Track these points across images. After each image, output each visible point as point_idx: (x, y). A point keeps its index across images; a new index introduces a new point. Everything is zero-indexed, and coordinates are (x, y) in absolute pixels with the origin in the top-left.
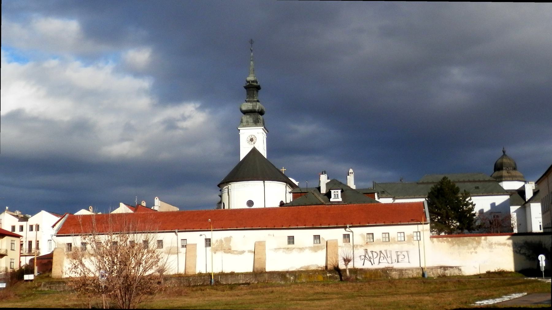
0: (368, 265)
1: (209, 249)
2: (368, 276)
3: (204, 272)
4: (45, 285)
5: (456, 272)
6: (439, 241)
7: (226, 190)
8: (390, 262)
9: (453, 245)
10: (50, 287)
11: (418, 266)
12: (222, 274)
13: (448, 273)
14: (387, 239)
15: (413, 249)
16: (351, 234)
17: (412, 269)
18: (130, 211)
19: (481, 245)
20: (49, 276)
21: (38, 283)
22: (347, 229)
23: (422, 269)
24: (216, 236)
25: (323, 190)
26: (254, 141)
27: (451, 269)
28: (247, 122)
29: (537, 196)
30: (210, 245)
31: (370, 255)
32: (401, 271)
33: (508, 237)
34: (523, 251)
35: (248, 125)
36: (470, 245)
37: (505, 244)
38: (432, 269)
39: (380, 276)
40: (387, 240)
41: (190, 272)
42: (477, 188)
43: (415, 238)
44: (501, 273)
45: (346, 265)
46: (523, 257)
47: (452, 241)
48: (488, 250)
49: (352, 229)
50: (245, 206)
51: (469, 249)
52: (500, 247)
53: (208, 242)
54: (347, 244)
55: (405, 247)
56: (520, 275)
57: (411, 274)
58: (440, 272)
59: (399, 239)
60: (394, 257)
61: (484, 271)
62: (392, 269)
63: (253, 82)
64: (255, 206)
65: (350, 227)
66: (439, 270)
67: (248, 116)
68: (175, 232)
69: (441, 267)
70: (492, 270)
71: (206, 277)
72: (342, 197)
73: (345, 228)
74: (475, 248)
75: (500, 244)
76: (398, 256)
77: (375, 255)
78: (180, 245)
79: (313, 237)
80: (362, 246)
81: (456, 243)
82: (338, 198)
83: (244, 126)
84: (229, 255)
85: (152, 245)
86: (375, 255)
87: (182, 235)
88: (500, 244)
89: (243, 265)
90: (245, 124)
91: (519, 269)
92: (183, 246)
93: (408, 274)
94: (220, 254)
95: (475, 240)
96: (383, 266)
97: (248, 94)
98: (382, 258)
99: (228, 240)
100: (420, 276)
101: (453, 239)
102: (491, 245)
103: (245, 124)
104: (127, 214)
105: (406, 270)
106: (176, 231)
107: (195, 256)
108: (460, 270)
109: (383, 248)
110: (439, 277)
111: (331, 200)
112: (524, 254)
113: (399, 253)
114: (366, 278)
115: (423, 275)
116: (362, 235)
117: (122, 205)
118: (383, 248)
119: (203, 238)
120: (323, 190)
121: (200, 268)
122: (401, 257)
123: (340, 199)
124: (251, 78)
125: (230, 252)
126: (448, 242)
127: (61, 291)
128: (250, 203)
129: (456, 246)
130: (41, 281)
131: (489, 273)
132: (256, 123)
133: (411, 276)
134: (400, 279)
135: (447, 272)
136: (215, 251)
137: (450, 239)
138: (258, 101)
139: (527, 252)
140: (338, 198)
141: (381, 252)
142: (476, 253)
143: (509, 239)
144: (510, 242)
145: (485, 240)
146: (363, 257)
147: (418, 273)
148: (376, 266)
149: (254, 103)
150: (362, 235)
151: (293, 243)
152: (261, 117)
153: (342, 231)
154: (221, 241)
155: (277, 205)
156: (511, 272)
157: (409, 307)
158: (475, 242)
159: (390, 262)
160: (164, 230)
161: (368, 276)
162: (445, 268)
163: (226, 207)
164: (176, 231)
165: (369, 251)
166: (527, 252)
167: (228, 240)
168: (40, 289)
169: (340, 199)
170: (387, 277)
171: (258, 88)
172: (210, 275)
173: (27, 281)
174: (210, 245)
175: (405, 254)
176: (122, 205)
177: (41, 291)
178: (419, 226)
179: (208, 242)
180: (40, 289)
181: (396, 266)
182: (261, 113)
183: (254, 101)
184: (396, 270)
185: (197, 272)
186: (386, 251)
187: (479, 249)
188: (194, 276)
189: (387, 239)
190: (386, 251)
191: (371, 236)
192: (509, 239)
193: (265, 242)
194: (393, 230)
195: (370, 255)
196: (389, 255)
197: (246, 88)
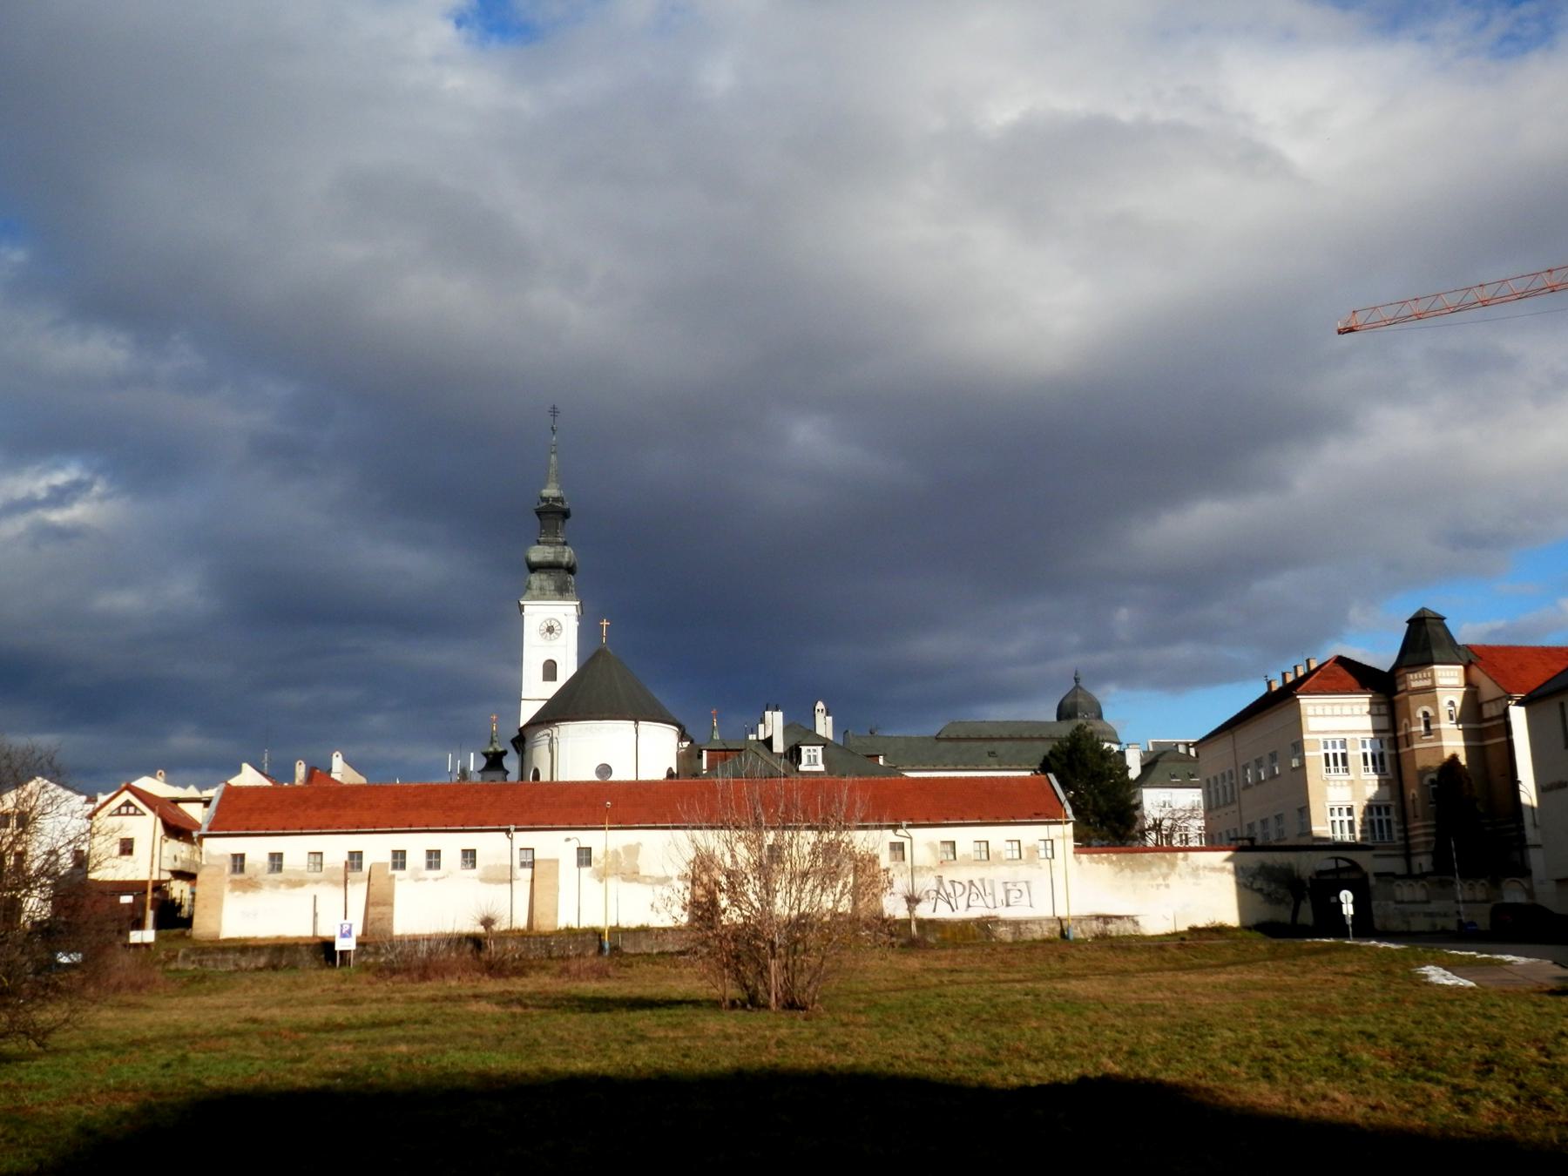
0: (943, 913)
1: (585, 870)
2: (948, 935)
3: (575, 926)
4: (186, 957)
5: (1128, 928)
6: (1093, 861)
7: (546, 740)
8: (991, 904)
9: (1122, 870)
10: (200, 962)
11: (1050, 914)
12: (616, 931)
13: (1113, 929)
14: (986, 854)
15: (1037, 876)
16: (907, 843)
17: (1038, 922)
18: (266, 783)
19: (1177, 870)
20: (183, 934)
21: (168, 951)
22: (900, 832)
23: (1060, 920)
24: (600, 841)
25: (779, 746)
26: (556, 628)
27: (1119, 922)
28: (541, 589)
29: (1154, 775)
30: (589, 863)
31: (950, 889)
32: (1016, 924)
33: (1228, 854)
34: (1257, 885)
35: (542, 595)
36: (1155, 870)
37: (1222, 869)
38: (1079, 920)
39: (974, 937)
40: (984, 856)
41: (544, 924)
42: (992, 754)
43: (1042, 854)
44: (1219, 931)
45: (911, 910)
46: (1259, 897)
47: (1119, 860)
48: (1190, 880)
49: (912, 831)
50: (593, 777)
51: (1153, 878)
52: (1213, 874)
53: (469, 856)
54: (472, 872)
55: (1023, 872)
56: (1259, 934)
57: (1039, 933)
58: (1096, 926)
59: (1009, 856)
60: (1000, 895)
61: (1183, 927)
62: (996, 921)
63: (556, 499)
64: (614, 778)
65: (909, 826)
66: (1094, 923)
67: (544, 576)
68: (508, 831)
69: (1098, 917)
70: (1201, 924)
71: (589, 937)
72: (825, 761)
73: (895, 828)
74: (1165, 877)
75: (1213, 869)
76: (1007, 891)
77: (959, 889)
78: (517, 863)
79: (460, 855)
80: (930, 869)
81: (1128, 866)
82: (809, 764)
83: (534, 598)
84: (635, 885)
85: (416, 859)
86: (959, 889)
87: (524, 839)
88: (1213, 869)
89: (338, 918)
90: (535, 593)
91: (1252, 921)
92: (523, 865)
93: (1031, 931)
94: (614, 883)
95: (1164, 858)
96: (976, 913)
97: (542, 527)
98: (973, 897)
99: (633, 851)
100: (1057, 935)
101: (1121, 856)
102: (1195, 870)
103: (535, 593)
104: (256, 789)
105: (1027, 922)
106: (512, 827)
107: (556, 887)
108: (1136, 923)
109: (975, 873)
110: (1096, 937)
111: (802, 768)
112: (1260, 890)
113: (1009, 886)
114: (944, 939)
115: (1063, 935)
116: (931, 845)
117: (246, 767)
118: (975, 873)
119: (574, 846)
120: (779, 746)
121: (566, 917)
122: (1014, 894)
123: (821, 767)
124: (551, 491)
125: (636, 880)
126: (1111, 862)
127: (230, 973)
128: (605, 770)
129: (1128, 872)
130: (174, 945)
131: (1194, 930)
132: (562, 592)
133: (1038, 936)
134: (1015, 942)
135: (1110, 927)
136: (602, 876)
137: (1114, 857)
138: (565, 544)
139: (1265, 886)
140: (809, 764)
141: (971, 882)
142: (1167, 886)
143: (1228, 860)
144: (1230, 866)
145: (1185, 859)
146: (933, 894)
147: (1052, 930)
148: (962, 914)
149: (559, 548)
150: (931, 845)
151: (438, 866)
152: (571, 578)
153: (889, 836)
154: (616, 853)
155: (662, 776)
156: (1231, 929)
157: (1552, 992)
158: (1165, 864)
159: (991, 904)
160: (358, 828)
161: (948, 935)
162: (1107, 919)
163: (545, 777)
164: (512, 827)
165: (946, 881)
166: (1265, 886)
167: (633, 851)
168: (173, 966)
169: (821, 767)
170: (988, 937)
171: (566, 514)
172: (596, 933)
173: (136, 945)
174: (589, 863)
175: (1023, 887)
176: (246, 767)
177: (177, 970)
178: (1051, 827)
179: (585, 857)
180: (173, 966)
181: (1004, 913)
182: (570, 570)
183: (558, 543)
184: (1005, 922)
185: (562, 924)
186: (982, 880)
187: (1173, 880)
188: (559, 933)
189: (1021, 854)
190: (982, 880)
191: (948, 847)
192: (1228, 860)
193: (557, 861)
194: (998, 836)
195: (950, 889)
196: (988, 890)
197: (539, 513)
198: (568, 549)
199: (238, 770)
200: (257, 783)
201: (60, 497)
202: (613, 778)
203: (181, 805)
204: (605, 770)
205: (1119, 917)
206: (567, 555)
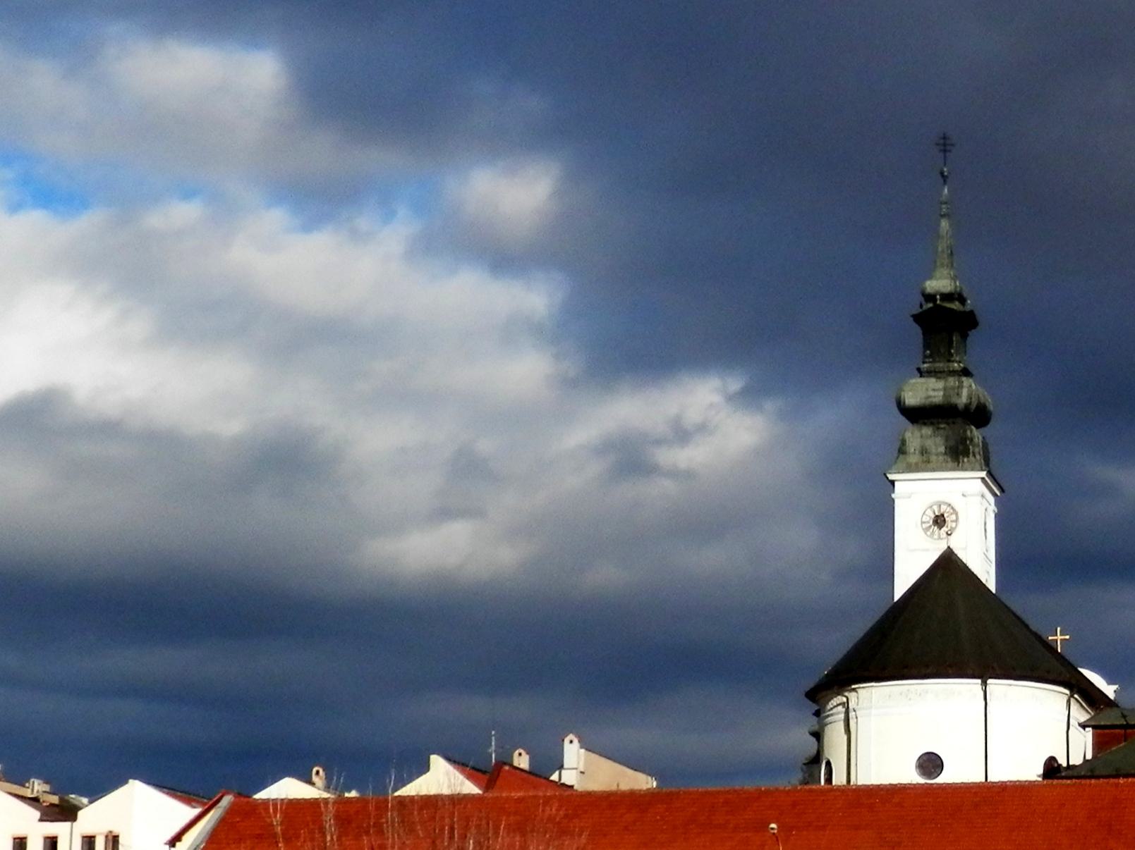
18: (470, 788)
35: (925, 463)
63: (948, 297)
67: (927, 431)
83: (911, 468)
90: (913, 459)
103: (913, 459)
104: (457, 801)
117: (437, 762)
124: (940, 283)
128: (930, 763)
132: (958, 454)
138: (966, 372)
149: (952, 381)
155: (1032, 772)
163: (839, 779)
176: (437, 762)
183: (953, 373)
198: (966, 381)
199: (424, 768)
200: (983, 577)
201: (339, 778)
202: (944, 778)
203: (197, 811)
204: (930, 763)
205: (10, 794)
206: (967, 392)
